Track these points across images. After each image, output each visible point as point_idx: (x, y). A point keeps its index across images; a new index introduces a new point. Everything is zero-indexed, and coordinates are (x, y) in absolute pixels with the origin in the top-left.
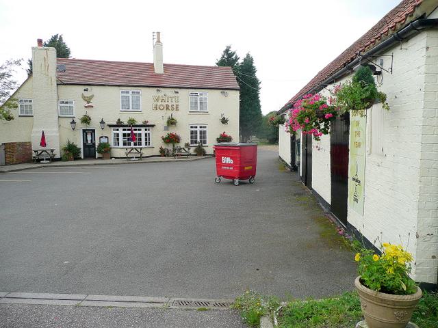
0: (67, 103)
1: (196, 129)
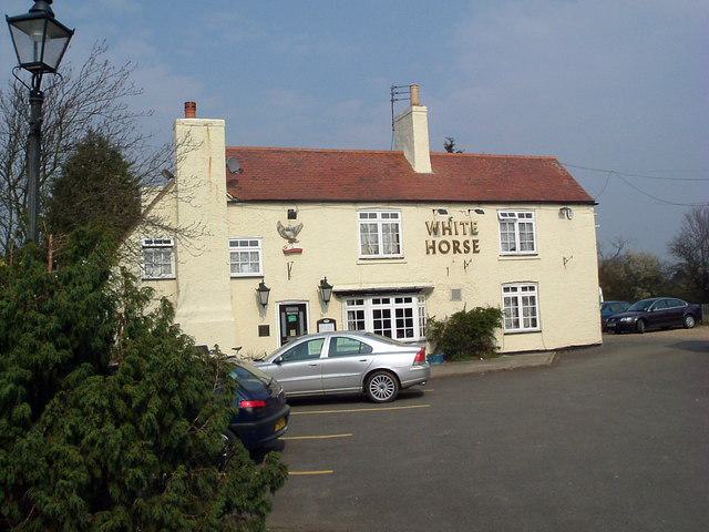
0: (244, 244)
1: (373, 221)
